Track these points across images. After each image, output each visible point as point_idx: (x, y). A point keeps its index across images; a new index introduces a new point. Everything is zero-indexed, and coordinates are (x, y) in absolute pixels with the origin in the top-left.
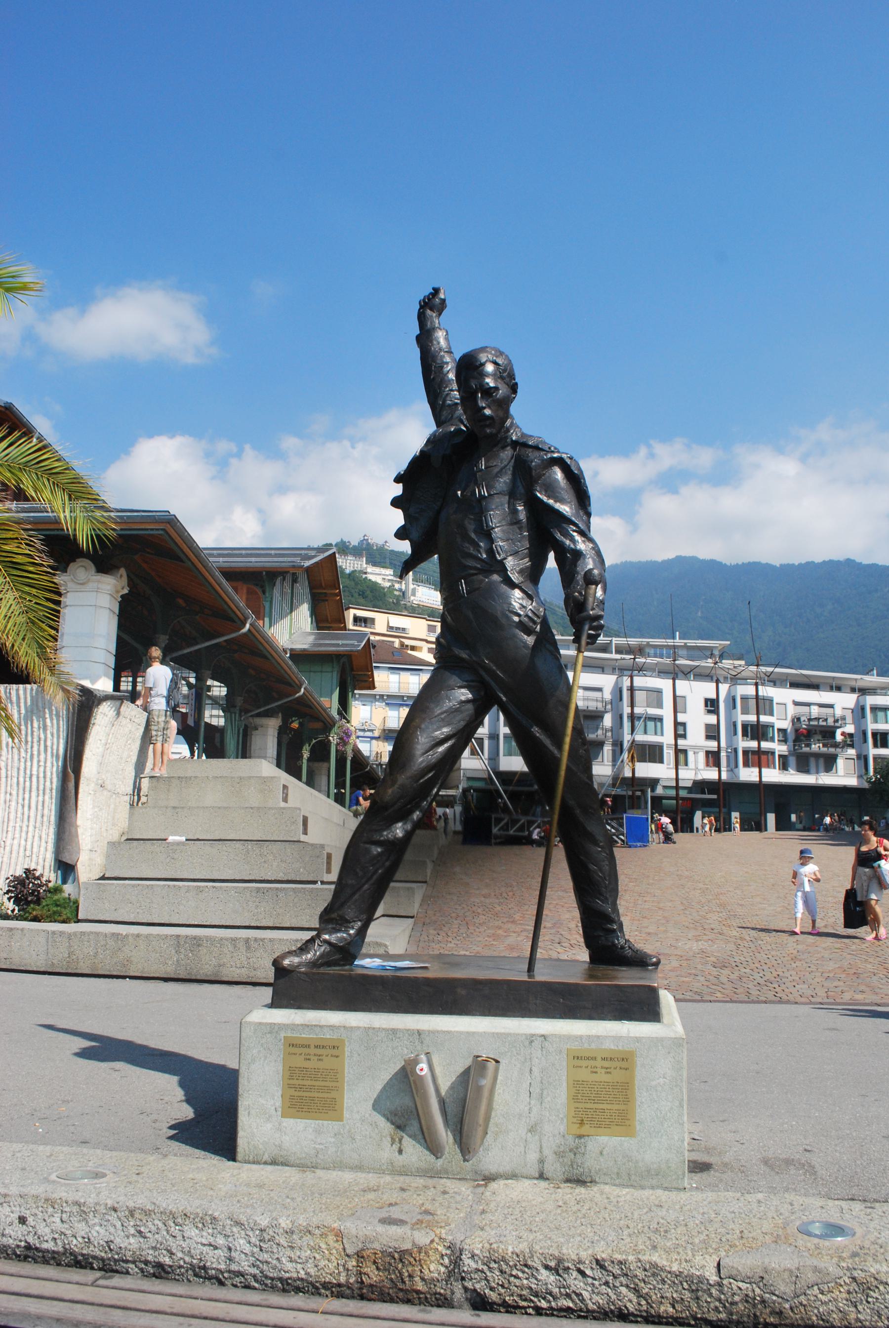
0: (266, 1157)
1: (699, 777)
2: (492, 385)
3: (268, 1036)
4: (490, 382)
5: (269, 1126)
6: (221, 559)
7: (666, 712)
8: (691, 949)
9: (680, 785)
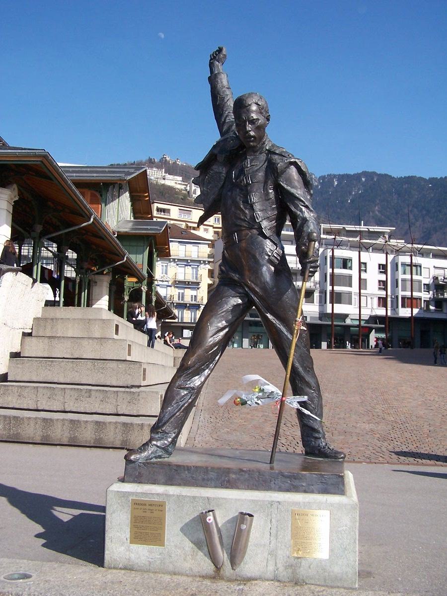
0: (121, 566)
1: (374, 314)
2: (255, 117)
3: (122, 498)
4: (254, 116)
5: (123, 548)
6: (74, 175)
7: (354, 272)
8: (365, 429)
9: (362, 318)
